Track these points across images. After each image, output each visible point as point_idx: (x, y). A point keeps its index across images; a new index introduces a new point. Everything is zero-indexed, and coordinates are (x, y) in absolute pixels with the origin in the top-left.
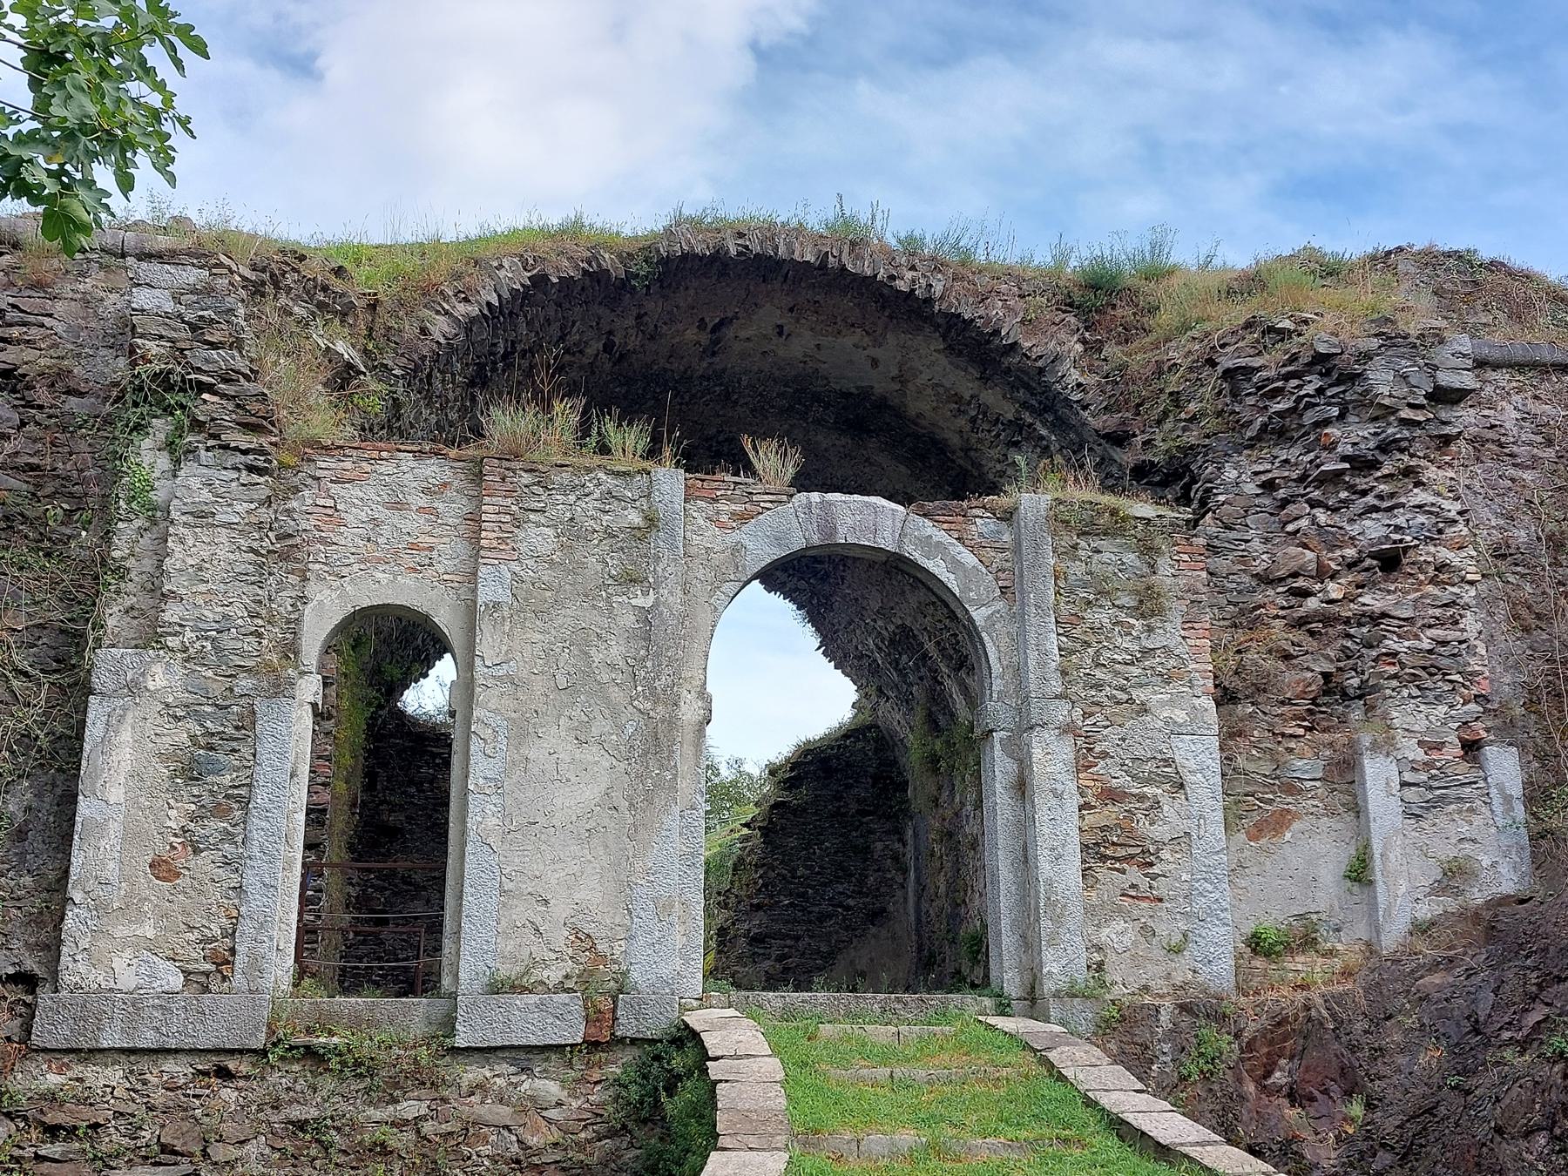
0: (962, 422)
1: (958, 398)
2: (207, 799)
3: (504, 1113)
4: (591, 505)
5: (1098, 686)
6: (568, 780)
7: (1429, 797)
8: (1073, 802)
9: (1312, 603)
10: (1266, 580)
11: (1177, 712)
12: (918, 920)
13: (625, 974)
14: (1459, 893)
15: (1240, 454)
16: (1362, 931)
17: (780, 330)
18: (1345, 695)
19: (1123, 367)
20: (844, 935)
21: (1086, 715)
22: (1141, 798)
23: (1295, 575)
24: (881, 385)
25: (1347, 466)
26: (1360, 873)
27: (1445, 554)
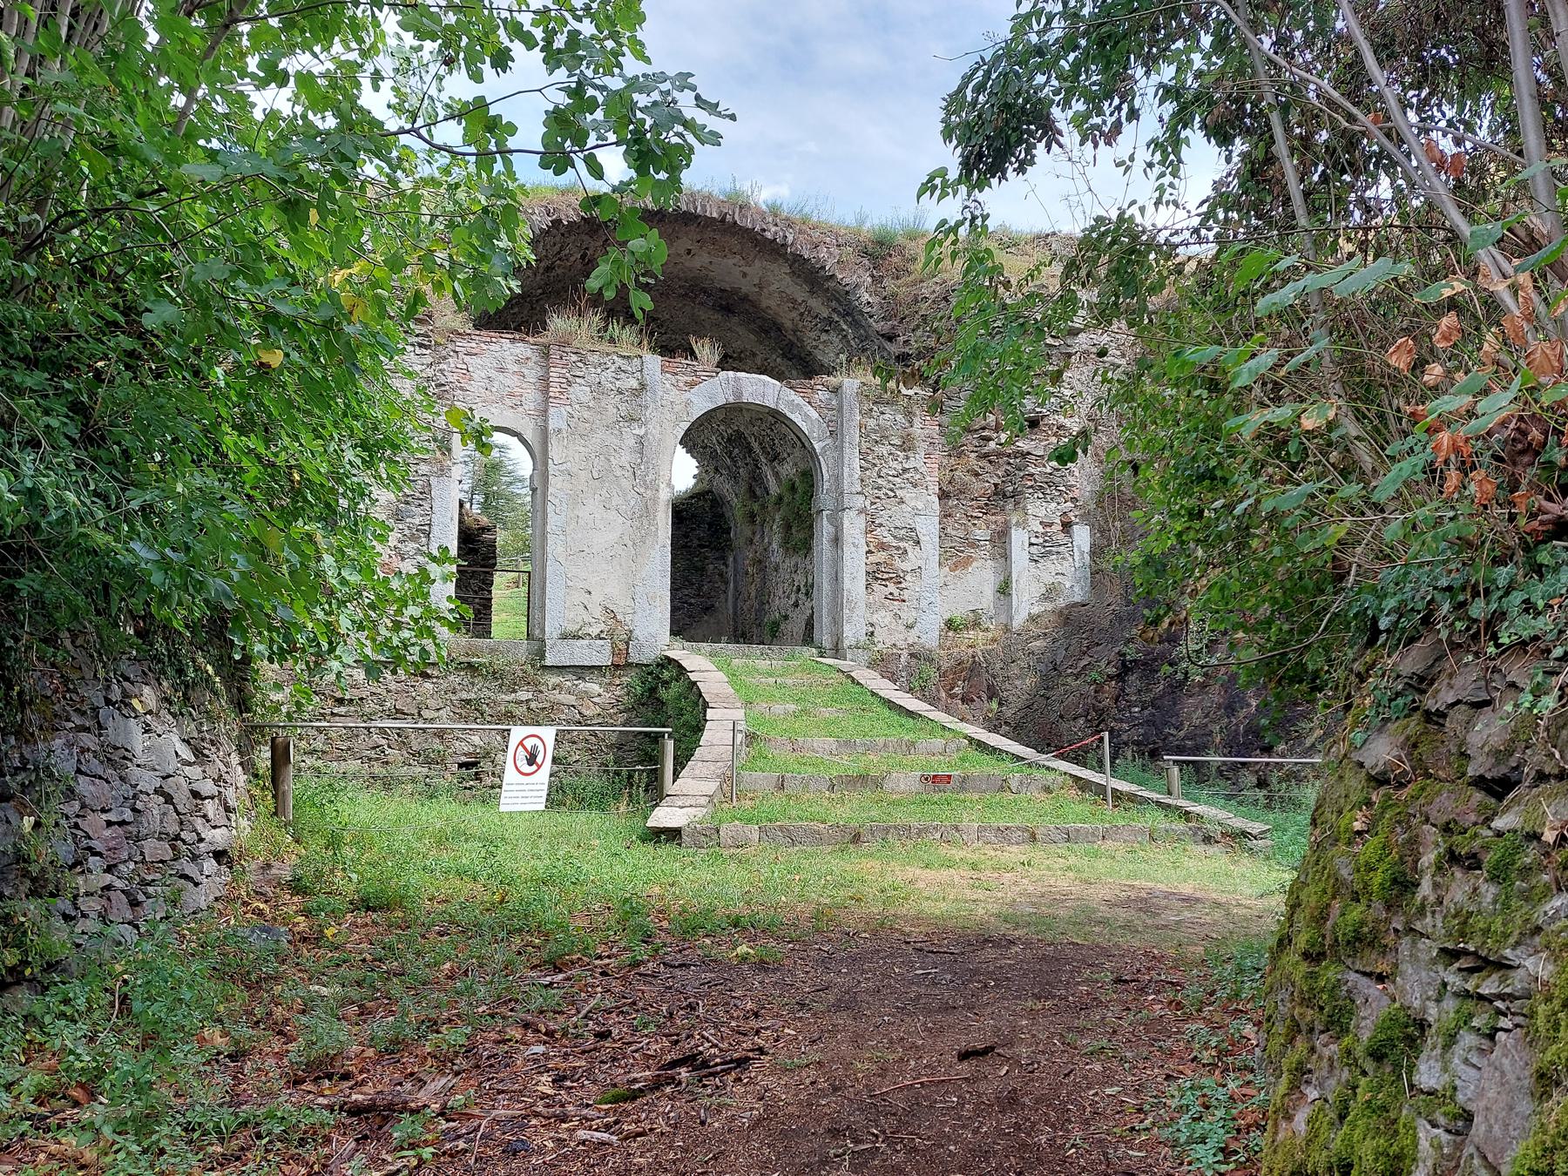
0: (794, 314)
1: (794, 301)
2: (407, 532)
3: (571, 699)
4: (609, 374)
7: (1044, 550)
9: (992, 444)
12: (735, 613)
14: (1053, 600)
16: (1003, 619)
17: (689, 252)
18: (1004, 496)
19: (895, 295)
20: (687, 620)
22: (898, 548)
24: (746, 287)
26: (1004, 590)
27: (1062, 419)
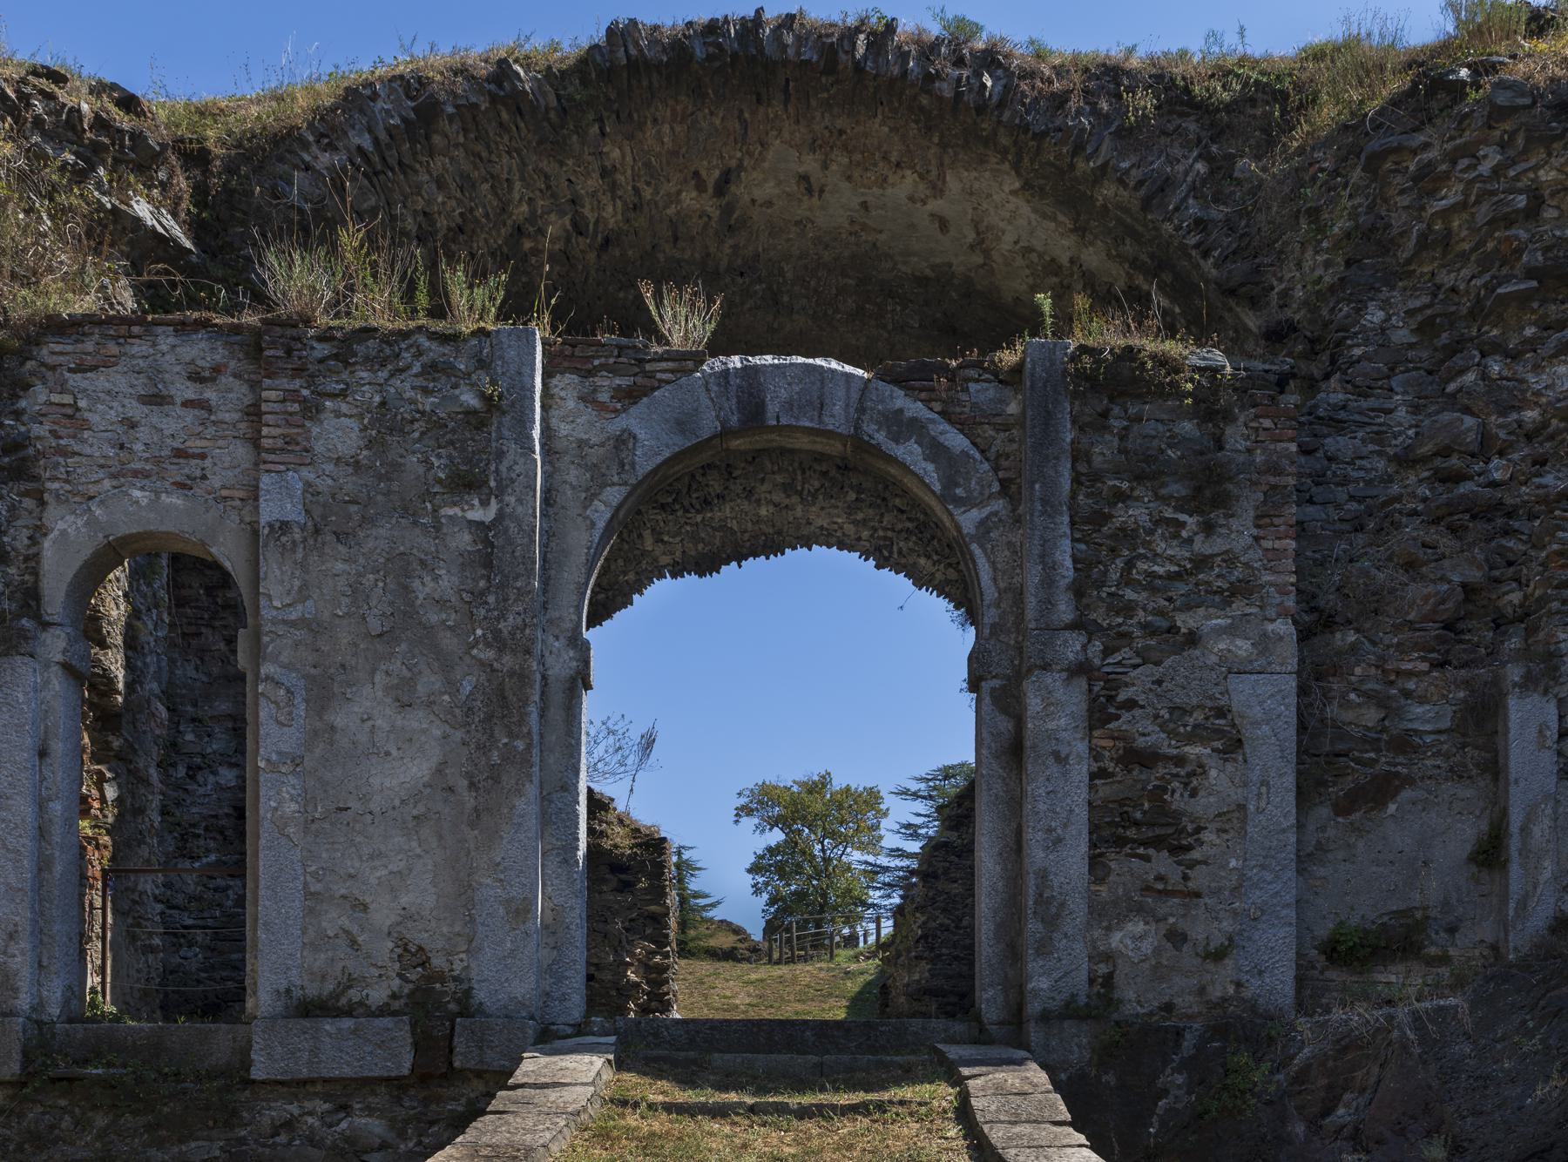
5: (1128, 609)
6: (388, 754)
8: (1080, 771)
10: (1406, 460)
11: (1239, 642)
13: (468, 993)
15: (1393, 288)
16: (1487, 931)
21: (1107, 652)
22: (1180, 761)
23: (1445, 452)
25: (1534, 284)
26: (1490, 854)
